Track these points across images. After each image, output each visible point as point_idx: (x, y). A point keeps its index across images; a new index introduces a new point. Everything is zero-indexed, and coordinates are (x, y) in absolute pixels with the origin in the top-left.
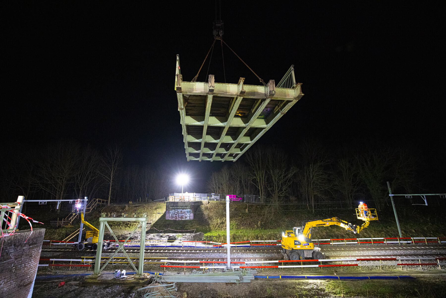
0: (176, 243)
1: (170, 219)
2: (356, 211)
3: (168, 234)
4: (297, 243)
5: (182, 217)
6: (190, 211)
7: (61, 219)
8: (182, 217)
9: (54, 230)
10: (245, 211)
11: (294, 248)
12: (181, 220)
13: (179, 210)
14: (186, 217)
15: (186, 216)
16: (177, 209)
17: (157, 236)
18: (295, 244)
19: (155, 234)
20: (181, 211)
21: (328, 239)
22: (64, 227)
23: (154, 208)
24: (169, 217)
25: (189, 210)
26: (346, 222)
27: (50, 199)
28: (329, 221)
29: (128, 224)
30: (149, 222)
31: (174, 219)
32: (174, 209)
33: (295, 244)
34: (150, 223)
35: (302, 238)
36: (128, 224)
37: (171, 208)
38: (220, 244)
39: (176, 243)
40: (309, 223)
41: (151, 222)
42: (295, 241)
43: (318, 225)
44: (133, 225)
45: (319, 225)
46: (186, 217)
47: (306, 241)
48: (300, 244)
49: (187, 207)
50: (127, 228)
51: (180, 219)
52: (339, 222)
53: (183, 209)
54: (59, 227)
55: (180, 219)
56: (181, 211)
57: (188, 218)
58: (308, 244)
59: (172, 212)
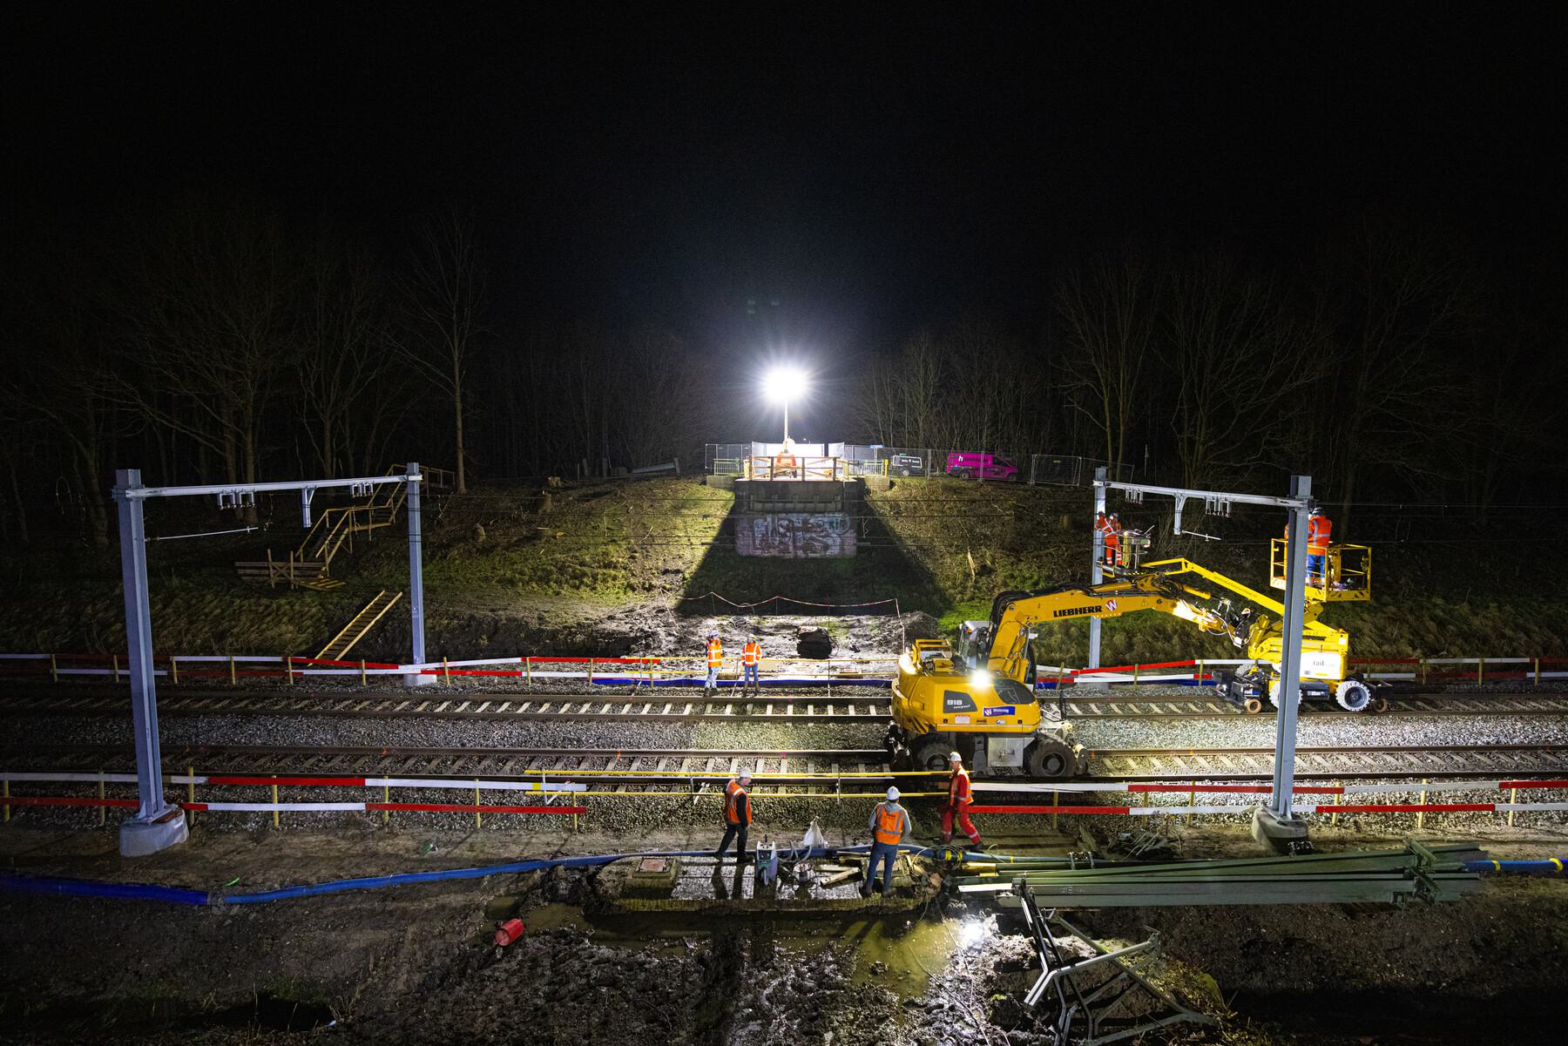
0: (843, 660)
1: (758, 553)
2: (1273, 550)
3: (800, 621)
4: (961, 702)
5: (807, 547)
6: (843, 523)
7: (281, 556)
8: (807, 547)
9: (264, 601)
10: (1056, 521)
11: (942, 727)
12: (808, 560)
13: (794, 517)
14: (826, 547)
15: (830, 542)
16: (787, 512)
17: (737, 626)
18: (948, 709)
19: (726, 621)
20: (805, 522)
21: (1473, 656)
22: (303, 589)
23: (668, 504)
24: (749, 544)
25: (839, 516)
26: (1207, 596)
27: (199, 483)
28: (1121, 593)
29: (584, 574)
30: (672, 566)
31: (774, 552)
32: (773, 512)
33: (948, 709)
34: (677, 572)
35: (980, 681)
36: (584, 574)
37: (759, 506)
38: (1068, 671)
39: (843, 660)
40: (1017, 603)
41: (680, 565)
42: (949, 695)
43: (1063, 613)
44: (605, 581)
45: (1071, 612)
46: (826, 547)
47: (1004, 697)
48: (974, 708)
49: (831, 506)
50: (585, 592)
51: (800, 553)
52: (1166, 595)
53: (813, 512)
54: (283, 588)
55: (800, 553)
56: (805, 522)
57: (834, 551)
58: (1012, 711)
59: (762, 524)
